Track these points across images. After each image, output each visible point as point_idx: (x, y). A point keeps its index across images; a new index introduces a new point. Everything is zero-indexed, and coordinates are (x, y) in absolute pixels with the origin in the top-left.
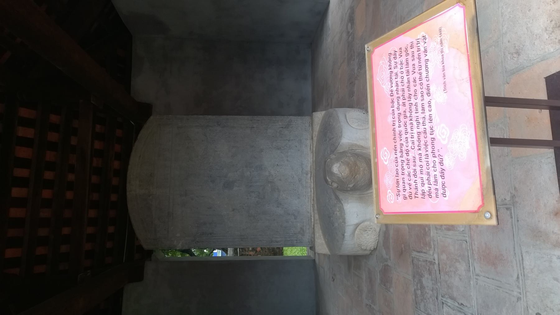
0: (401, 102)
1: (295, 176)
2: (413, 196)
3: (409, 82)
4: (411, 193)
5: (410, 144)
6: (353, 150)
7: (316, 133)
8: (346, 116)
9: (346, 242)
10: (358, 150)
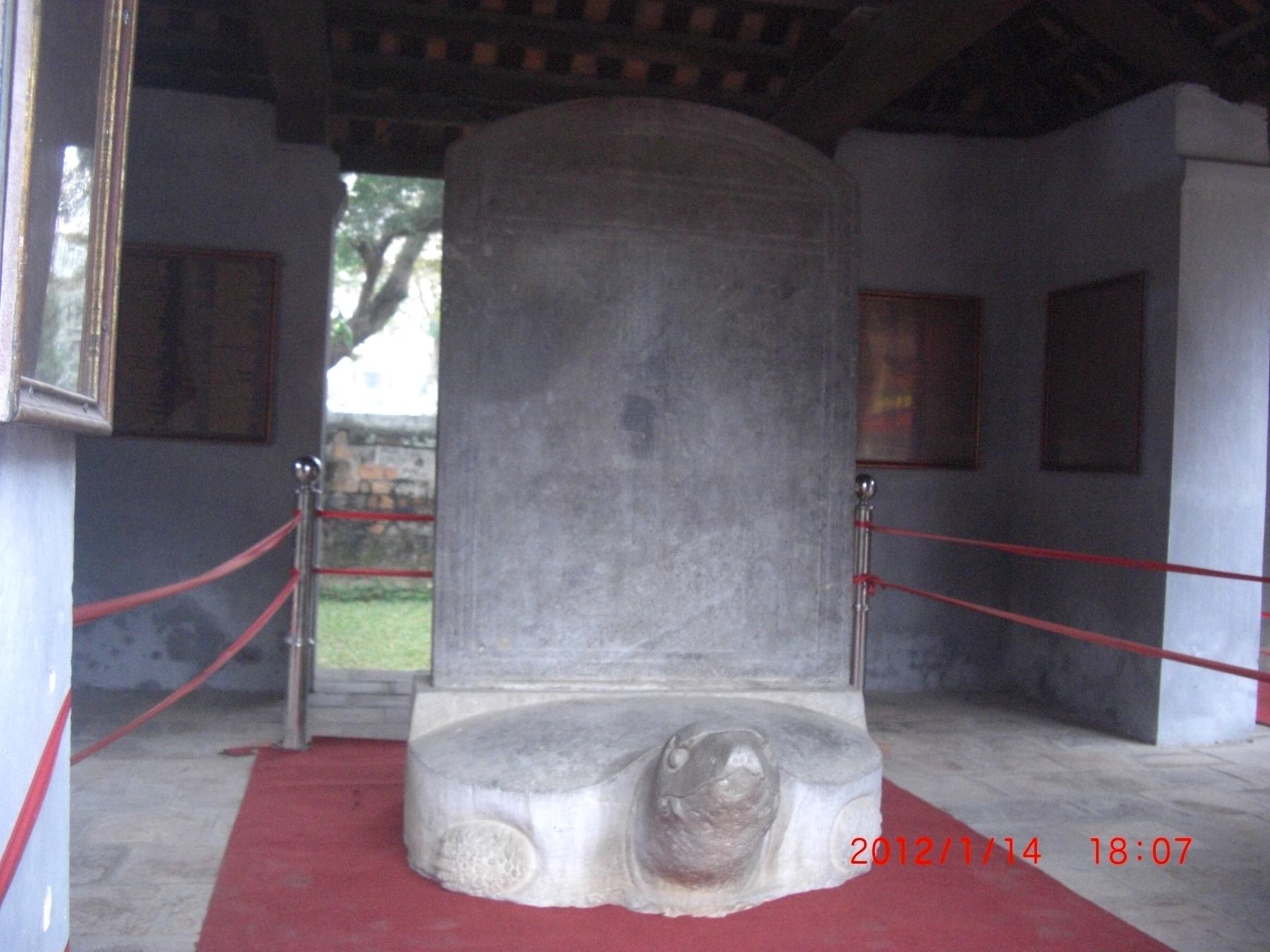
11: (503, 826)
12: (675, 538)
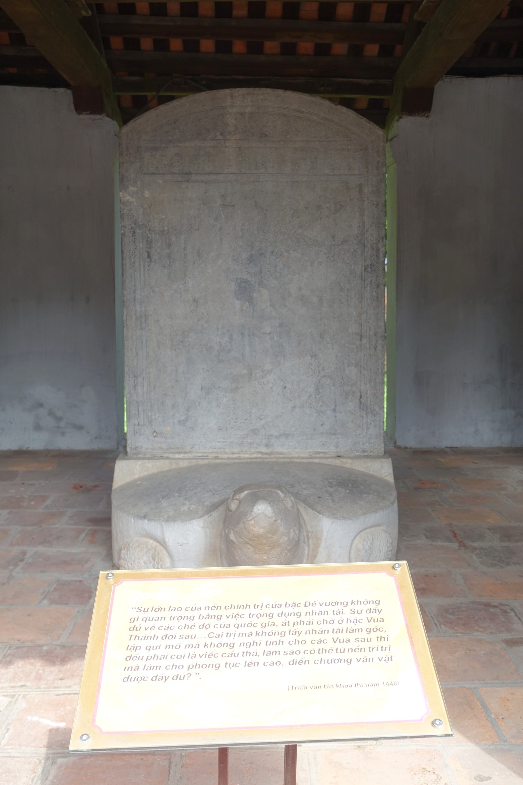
0: (292, 619)
1: (263, 422)
2: (134, 633)
3: (322, 632)
4: (238, 656)
5: (219, 631)
6: (308, 540)
7: (348, 464)
8: (379, 525)
9: (133, 521)
10: (307, 549)
11: (151, 541)
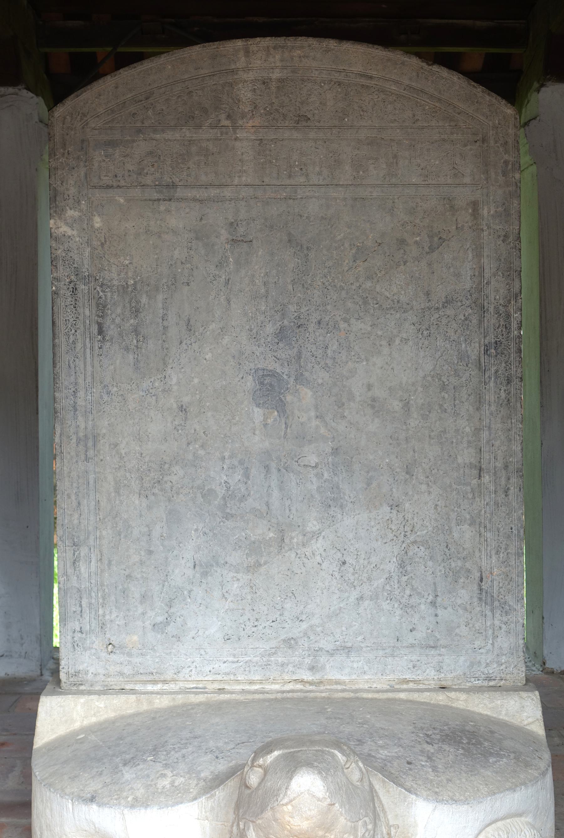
1: (304, 626)
8: (520, 815)
9: (70, 806)
12: (315, 523)
